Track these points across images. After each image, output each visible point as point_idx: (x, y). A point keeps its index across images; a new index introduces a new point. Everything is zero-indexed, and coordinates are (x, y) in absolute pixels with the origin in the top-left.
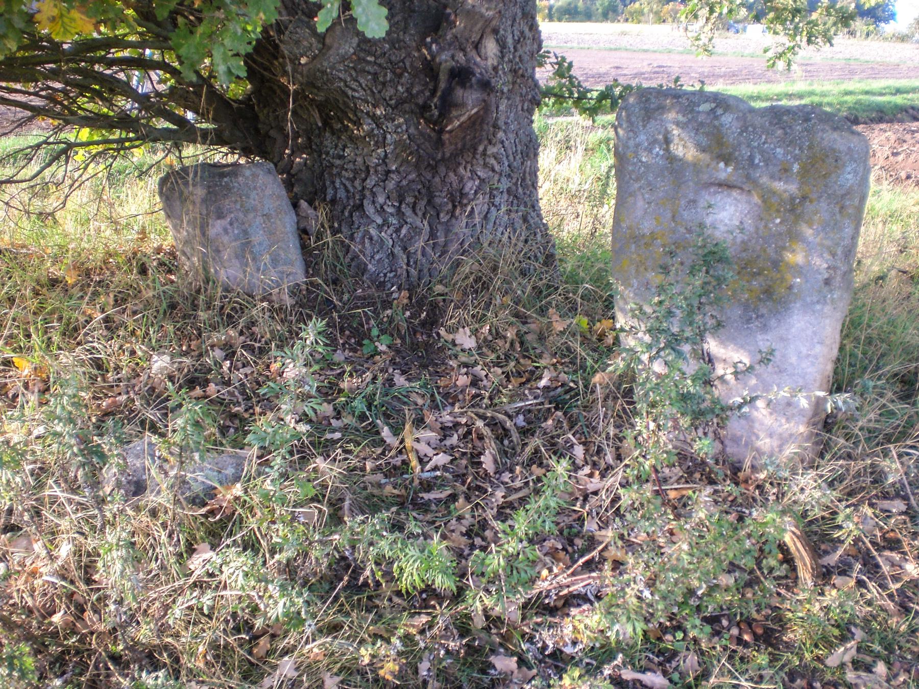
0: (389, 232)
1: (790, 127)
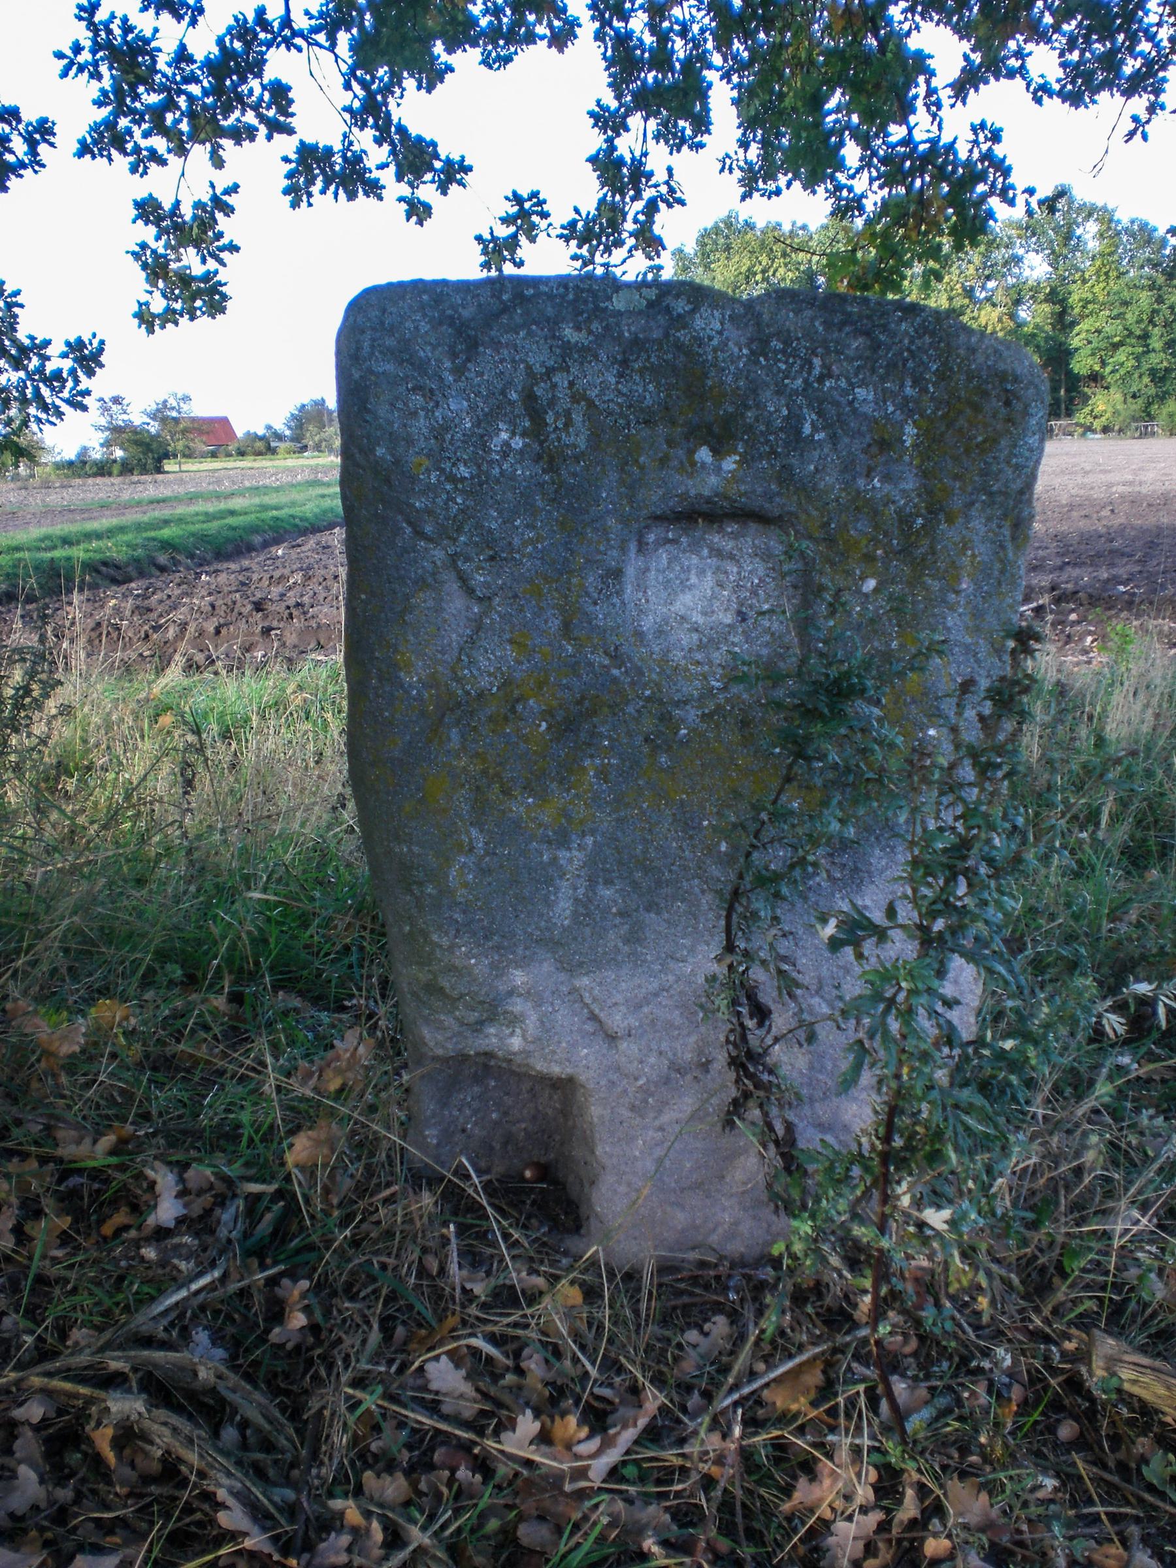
1: (885, 328)
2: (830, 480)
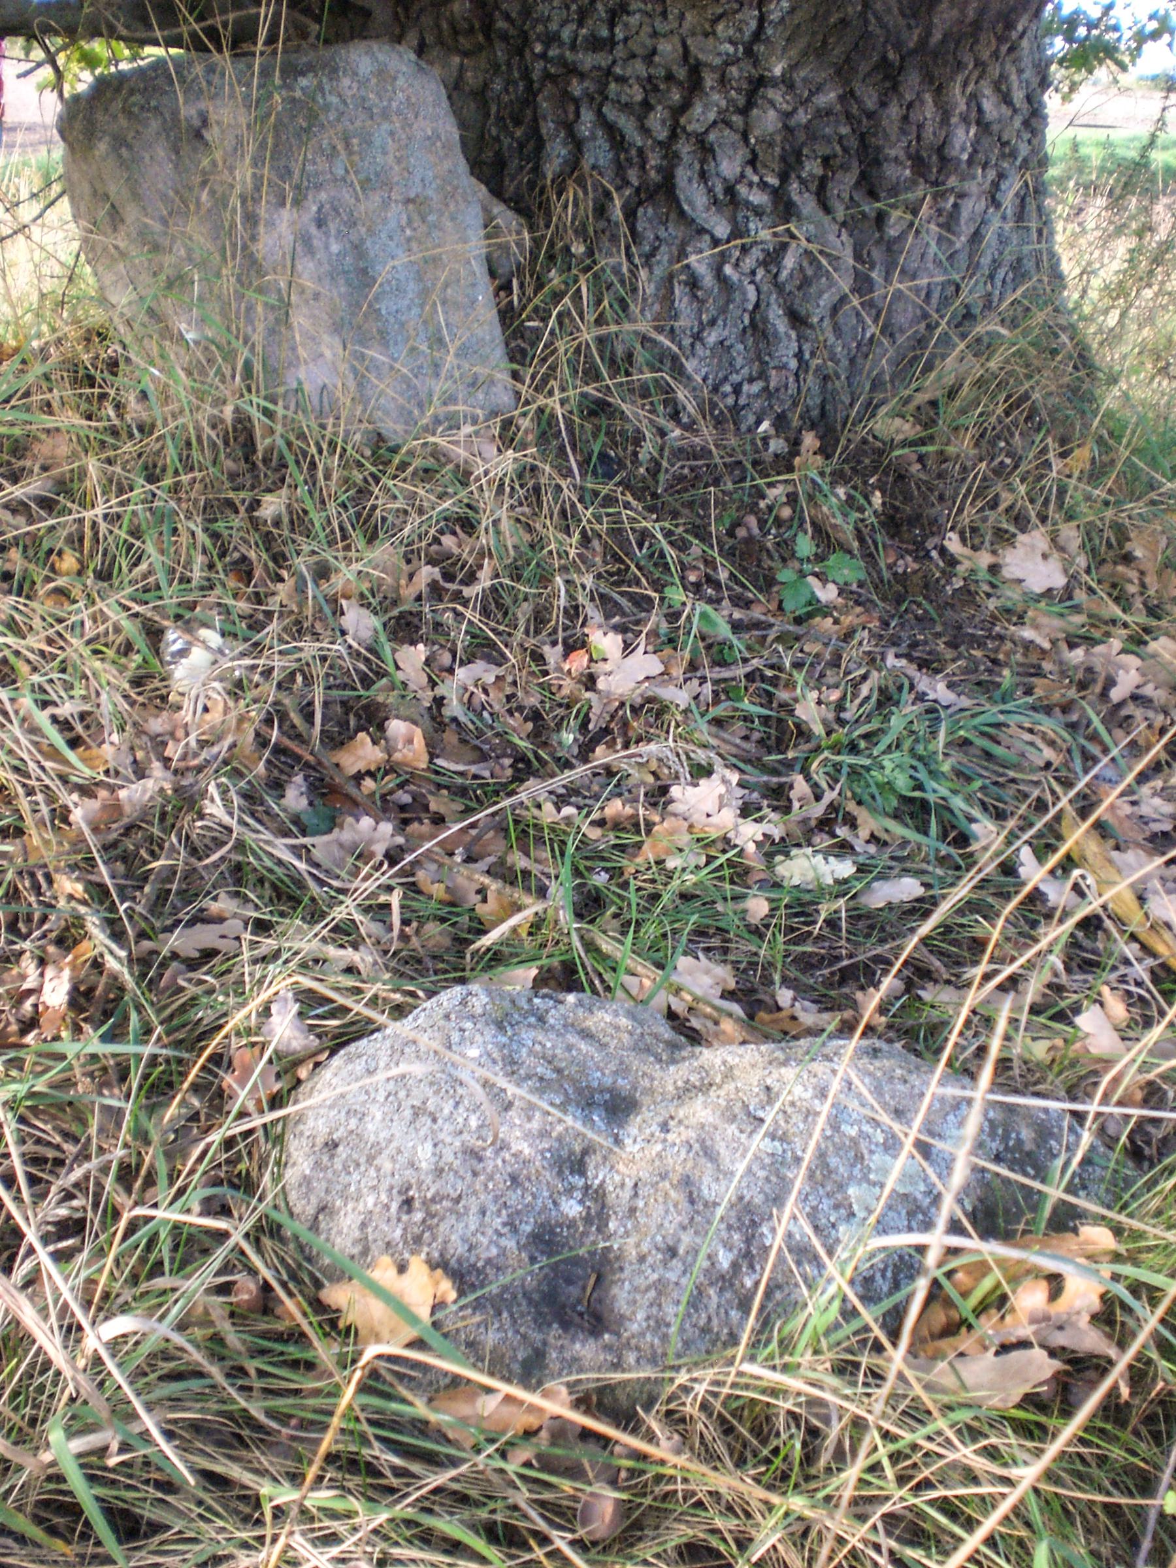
0: (749, 263)
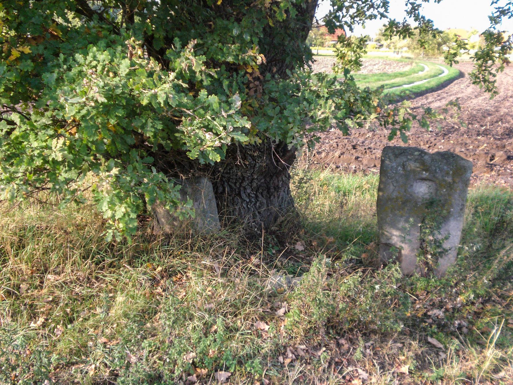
2: (440, 177)
